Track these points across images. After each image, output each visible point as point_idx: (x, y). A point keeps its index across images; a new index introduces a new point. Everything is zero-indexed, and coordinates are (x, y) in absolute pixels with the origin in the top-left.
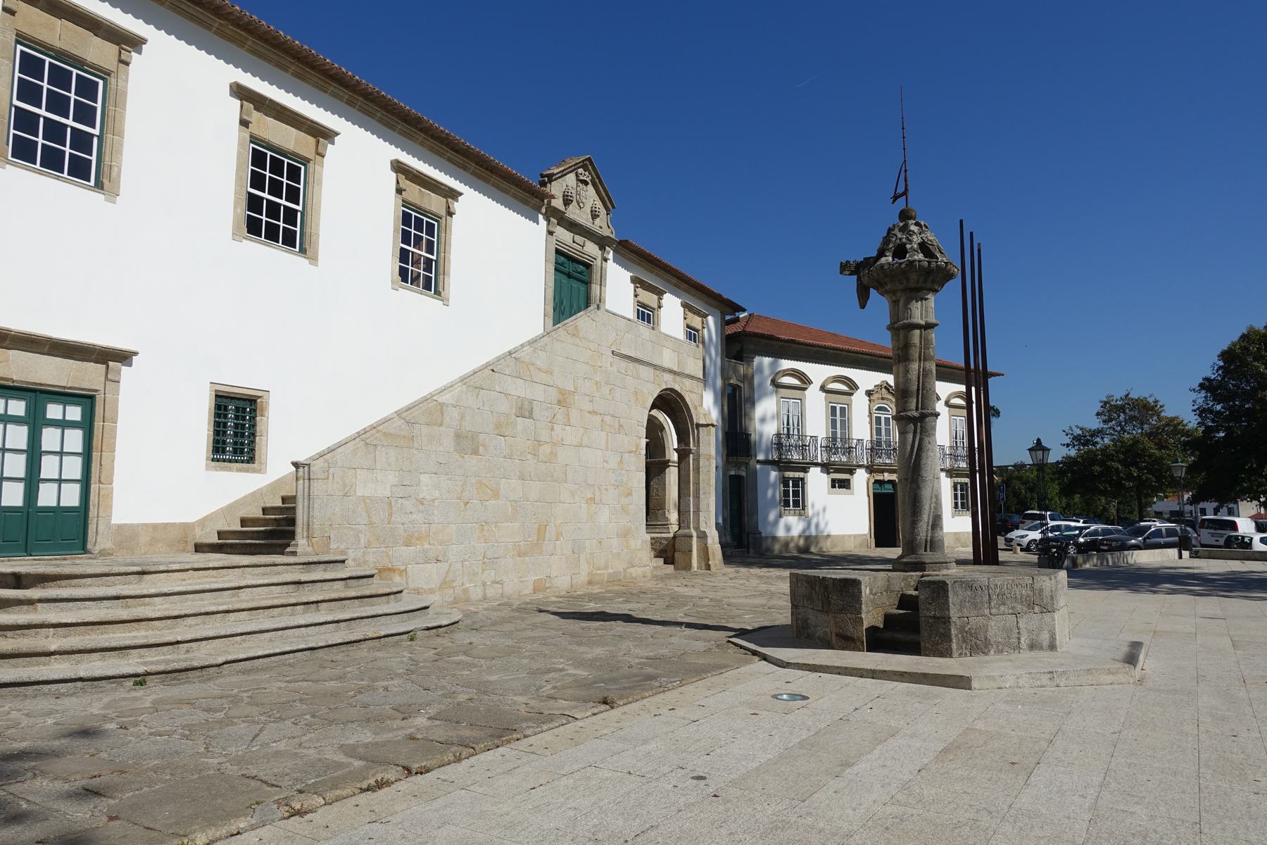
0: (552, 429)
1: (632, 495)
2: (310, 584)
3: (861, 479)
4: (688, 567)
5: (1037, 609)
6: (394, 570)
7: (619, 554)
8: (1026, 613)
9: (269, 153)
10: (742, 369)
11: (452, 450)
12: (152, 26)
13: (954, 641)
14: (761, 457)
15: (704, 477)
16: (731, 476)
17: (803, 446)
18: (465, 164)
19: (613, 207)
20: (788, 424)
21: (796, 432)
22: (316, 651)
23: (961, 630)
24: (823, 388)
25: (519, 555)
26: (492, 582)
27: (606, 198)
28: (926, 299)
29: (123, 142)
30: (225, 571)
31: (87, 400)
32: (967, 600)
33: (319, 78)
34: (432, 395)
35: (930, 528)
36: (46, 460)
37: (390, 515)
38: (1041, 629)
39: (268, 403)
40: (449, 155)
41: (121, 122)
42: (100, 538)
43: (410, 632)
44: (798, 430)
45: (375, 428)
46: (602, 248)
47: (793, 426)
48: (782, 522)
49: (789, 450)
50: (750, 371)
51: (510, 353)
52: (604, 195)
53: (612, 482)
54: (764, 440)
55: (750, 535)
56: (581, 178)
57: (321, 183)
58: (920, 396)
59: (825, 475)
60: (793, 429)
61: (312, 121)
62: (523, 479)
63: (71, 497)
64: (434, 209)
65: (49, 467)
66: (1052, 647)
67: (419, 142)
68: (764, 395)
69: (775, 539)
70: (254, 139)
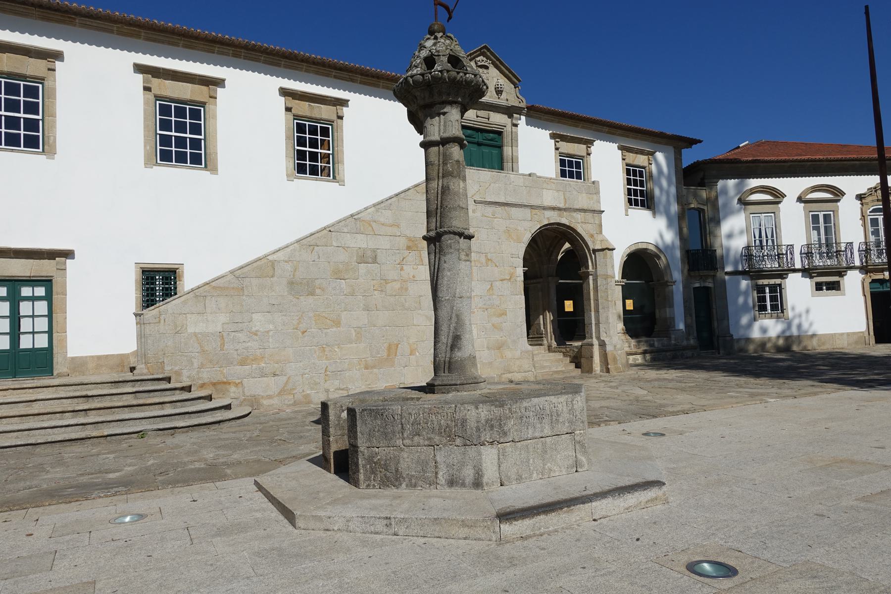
0: (402, 269)
1: (506, 315)
2: (99, 397)
3: (854, 281)
4: (590, 370)
5: (458, 441)
6: (229, 383)
7: (491, 363)
8: (445, 445)
9: (173, 105)
10: (704, 194)
11: (286, 293)
12: (61, 40)
13: (362, 471)
14: (729, 269)
15: (603, 294)
16: (695, 288)
17: (779, 255)
18: (351, 77)
19: (519, 81)
20: (760, 236)
21: (770, 243)
22: (37, 446)
23: (370, 460)
24: (800, 199)
25: (366, 368)
27: (510, 75)
28: (444, 114)
29: (56, 120)
30: (39, 390)
31: (47, 282)
32: (376, 430)
33: (204, 44)
34: (266, 256)
35: (448, 349)
36: (23, 321)
37: (223, 344)
38: (463, 464)
39: (183, 272)
40: (333, 74)
41: (53, 107)
42: (58, 367)
43: (141, 431)
44: (773, 241)
45: (208, 284)
46: (510, 116)
48: (757, 325)
49: (763, 260)
50: (713, 194)
51: (352, 216)
52: (508, 73)
53: (480, 305)
54: (732, 253)
56: (479, 64)
57: (216, 117)
59: (808, 279)
60: (767, 241)
61: (199, 76)
62: (368, 310)
63: (42, 342)
64: (324, 116)
65: (26, 325)
66: (477, 484)
67: (304, 70)
68: (730, 213)
69: (749, 340)
70: (157, 98)
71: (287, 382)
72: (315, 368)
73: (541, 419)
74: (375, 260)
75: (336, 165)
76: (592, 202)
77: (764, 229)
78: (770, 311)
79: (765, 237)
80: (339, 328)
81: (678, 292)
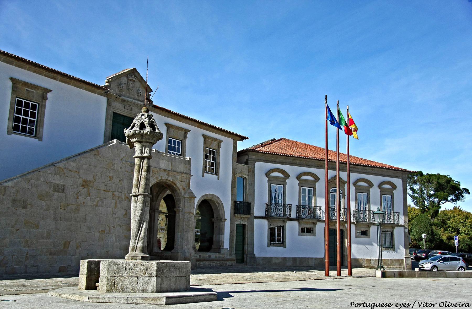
0: (78, 198)
11: (10, 206)
21: (273, 202)
25: (50, 254)
26: (31, 266)
47: (272, 198)
55: (248, 256)
58: (140, 176)
60: (278, 201)
62: (56, 220)
71: (3, 259)
72: (21, 252)
73: (176, 270)
74: (63, 191)
75: (38, 128)
76: (186, 169)
77: (277, 193)
78: (276, 242)
79: (277, 198)
80: (38, 229)
81: (227, 226)
